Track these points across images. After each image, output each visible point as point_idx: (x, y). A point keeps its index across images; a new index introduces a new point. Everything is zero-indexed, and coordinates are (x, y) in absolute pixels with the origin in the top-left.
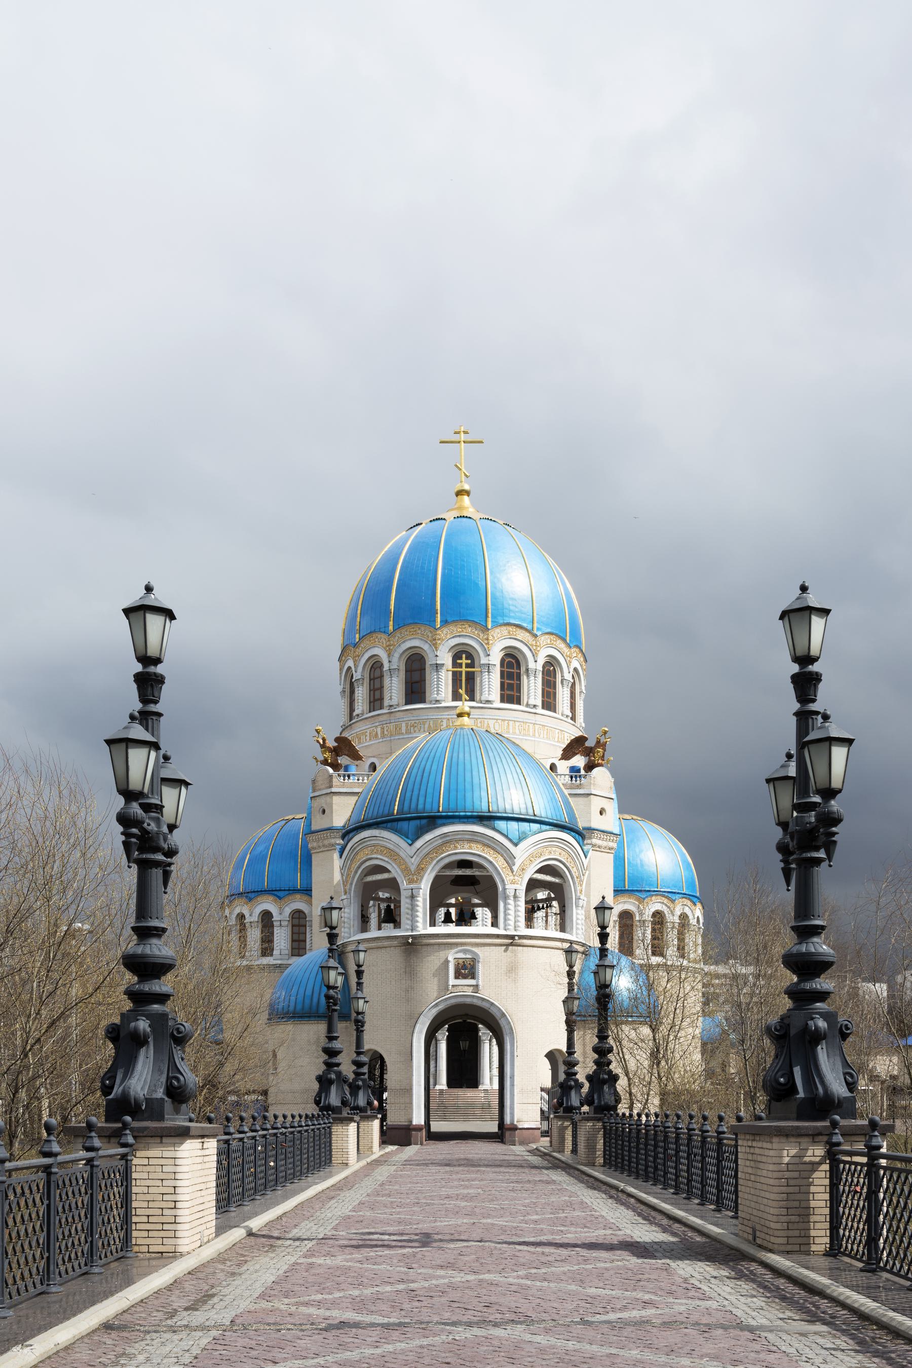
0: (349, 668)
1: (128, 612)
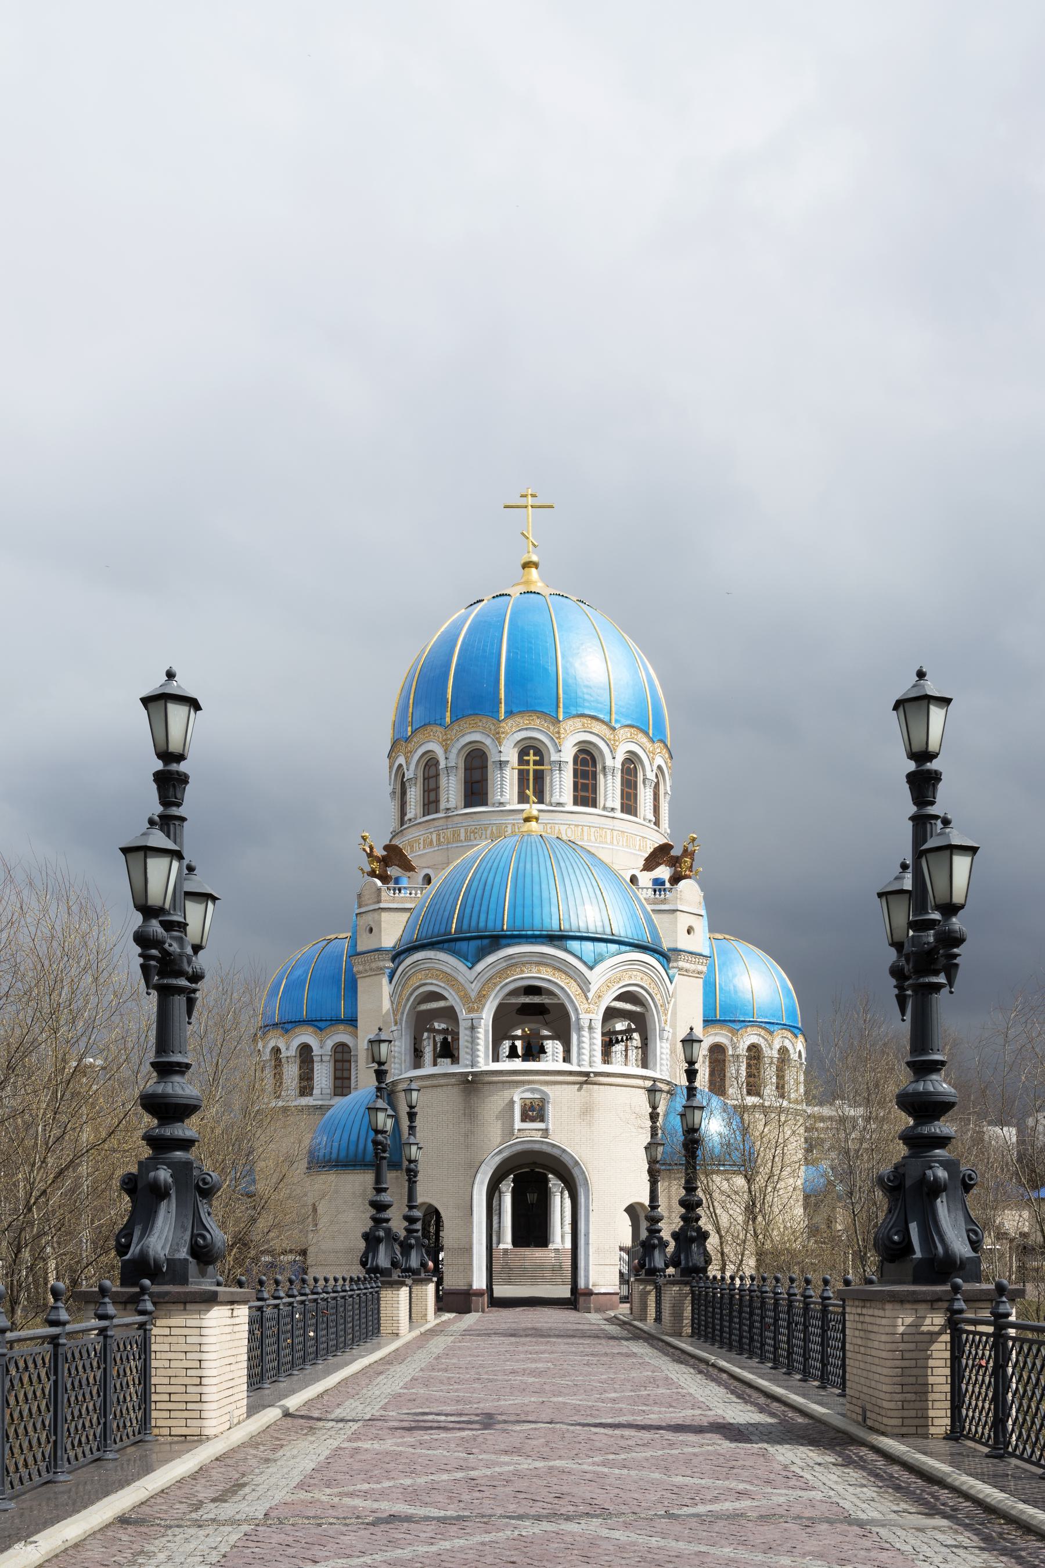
0: (400, 766)
1: (146, 701)
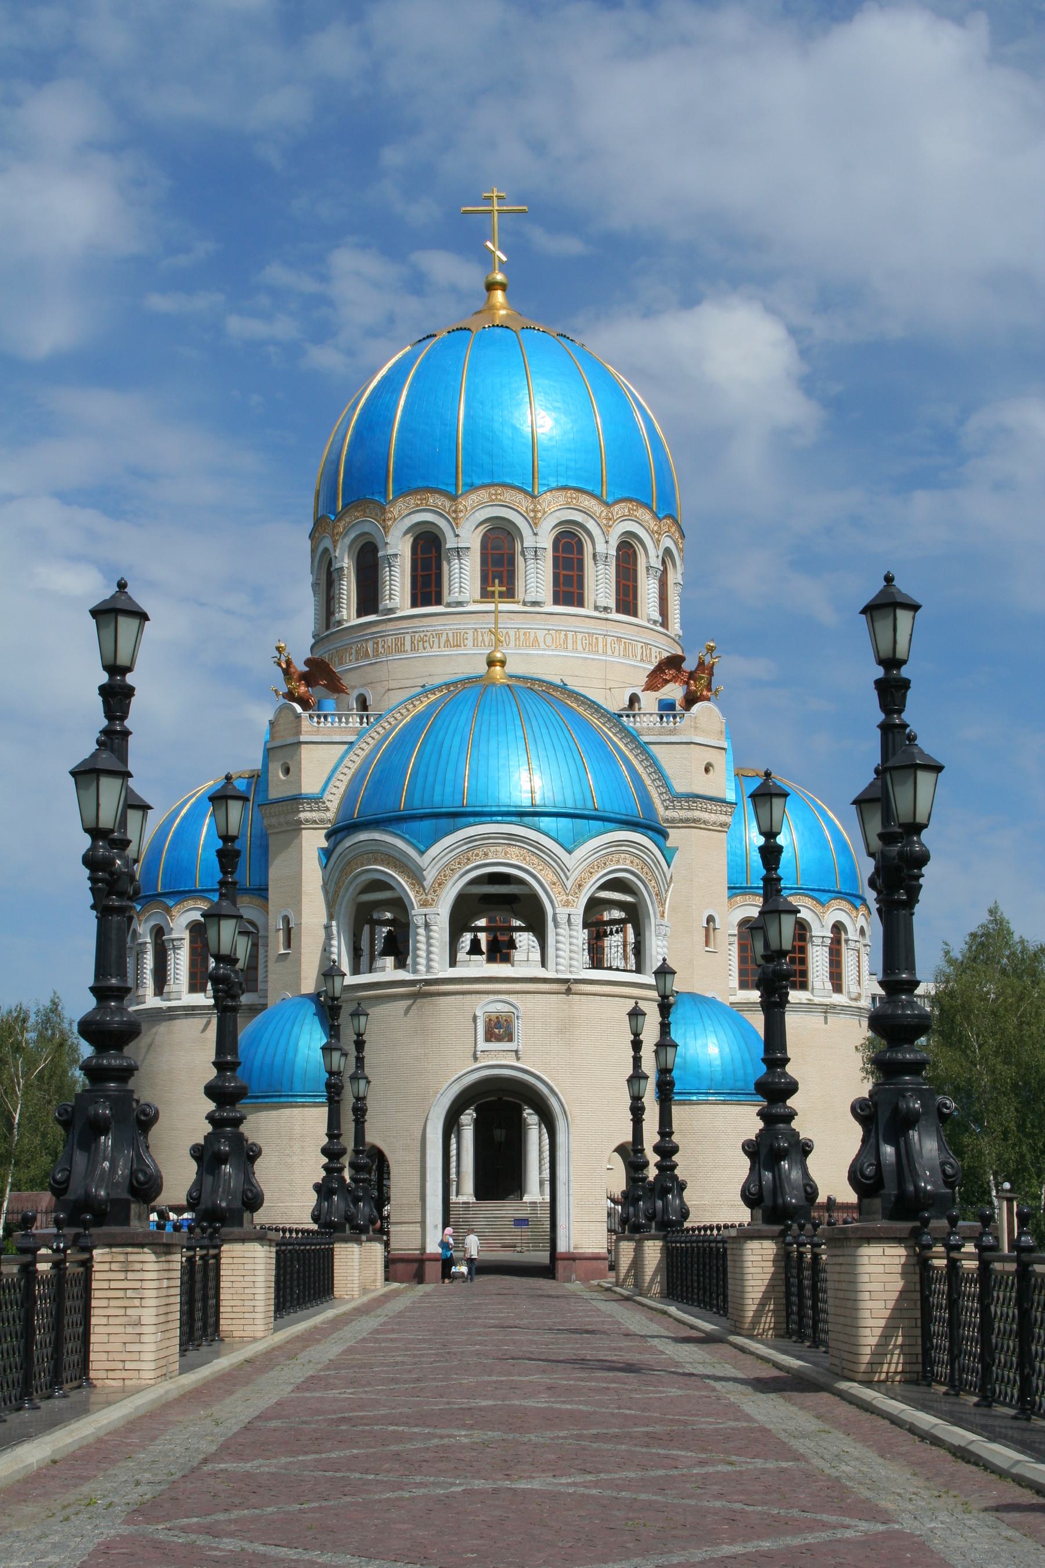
0: (326, 550)
1: (95, 613)
